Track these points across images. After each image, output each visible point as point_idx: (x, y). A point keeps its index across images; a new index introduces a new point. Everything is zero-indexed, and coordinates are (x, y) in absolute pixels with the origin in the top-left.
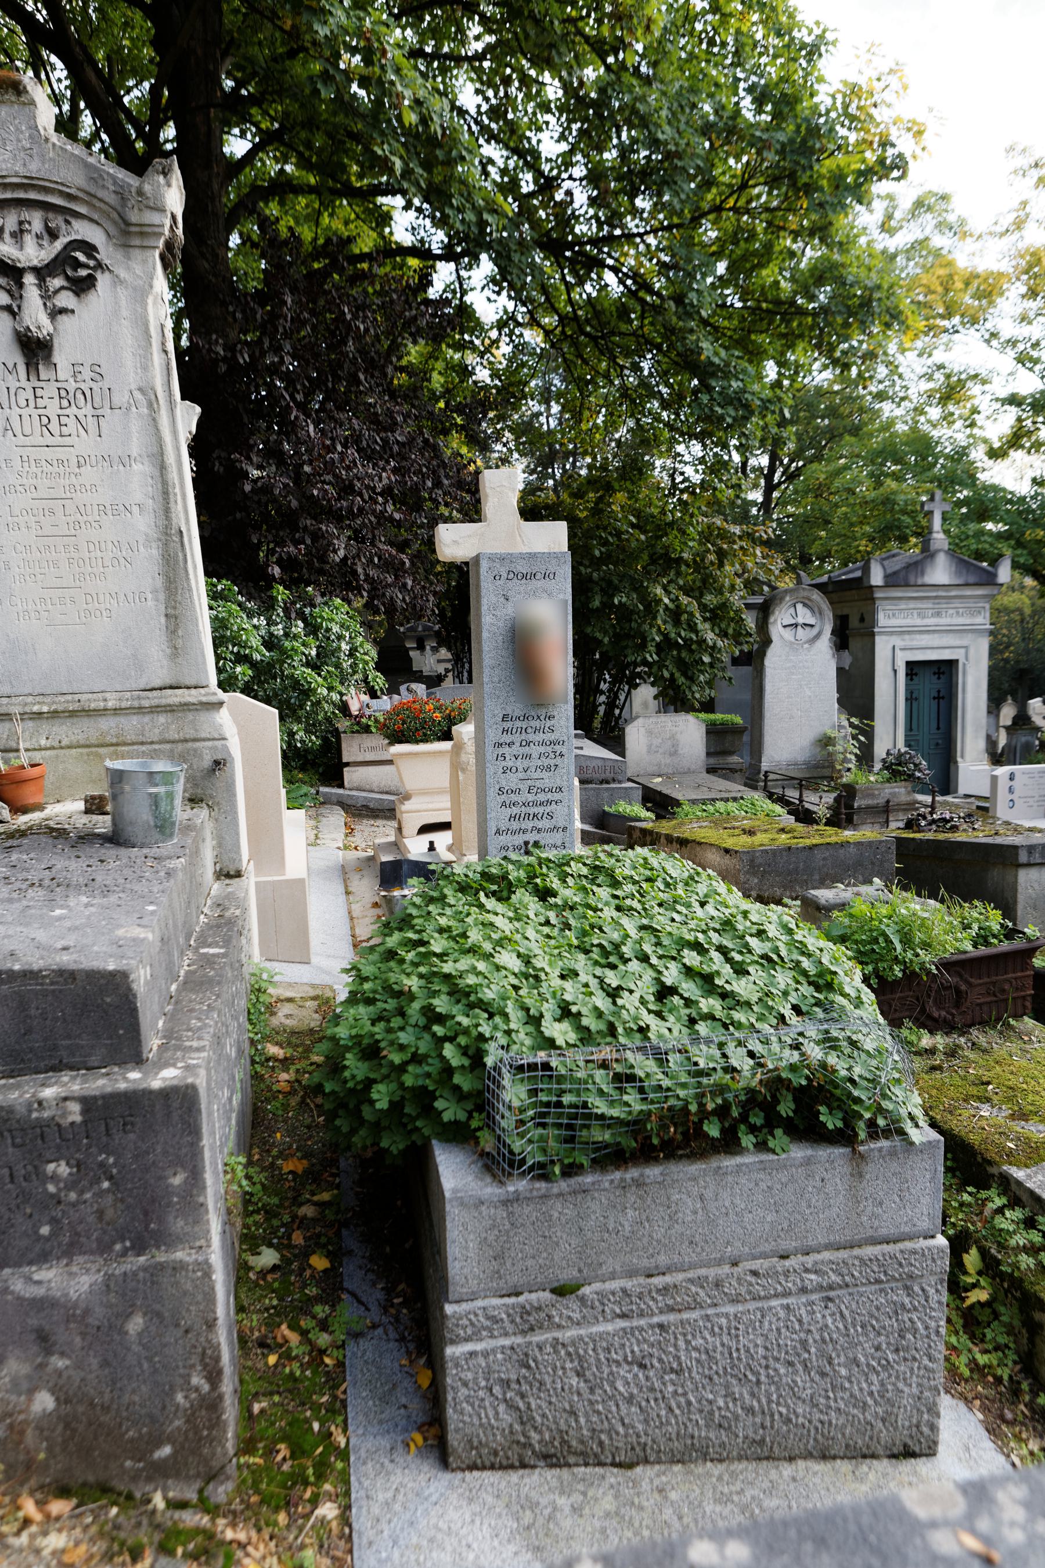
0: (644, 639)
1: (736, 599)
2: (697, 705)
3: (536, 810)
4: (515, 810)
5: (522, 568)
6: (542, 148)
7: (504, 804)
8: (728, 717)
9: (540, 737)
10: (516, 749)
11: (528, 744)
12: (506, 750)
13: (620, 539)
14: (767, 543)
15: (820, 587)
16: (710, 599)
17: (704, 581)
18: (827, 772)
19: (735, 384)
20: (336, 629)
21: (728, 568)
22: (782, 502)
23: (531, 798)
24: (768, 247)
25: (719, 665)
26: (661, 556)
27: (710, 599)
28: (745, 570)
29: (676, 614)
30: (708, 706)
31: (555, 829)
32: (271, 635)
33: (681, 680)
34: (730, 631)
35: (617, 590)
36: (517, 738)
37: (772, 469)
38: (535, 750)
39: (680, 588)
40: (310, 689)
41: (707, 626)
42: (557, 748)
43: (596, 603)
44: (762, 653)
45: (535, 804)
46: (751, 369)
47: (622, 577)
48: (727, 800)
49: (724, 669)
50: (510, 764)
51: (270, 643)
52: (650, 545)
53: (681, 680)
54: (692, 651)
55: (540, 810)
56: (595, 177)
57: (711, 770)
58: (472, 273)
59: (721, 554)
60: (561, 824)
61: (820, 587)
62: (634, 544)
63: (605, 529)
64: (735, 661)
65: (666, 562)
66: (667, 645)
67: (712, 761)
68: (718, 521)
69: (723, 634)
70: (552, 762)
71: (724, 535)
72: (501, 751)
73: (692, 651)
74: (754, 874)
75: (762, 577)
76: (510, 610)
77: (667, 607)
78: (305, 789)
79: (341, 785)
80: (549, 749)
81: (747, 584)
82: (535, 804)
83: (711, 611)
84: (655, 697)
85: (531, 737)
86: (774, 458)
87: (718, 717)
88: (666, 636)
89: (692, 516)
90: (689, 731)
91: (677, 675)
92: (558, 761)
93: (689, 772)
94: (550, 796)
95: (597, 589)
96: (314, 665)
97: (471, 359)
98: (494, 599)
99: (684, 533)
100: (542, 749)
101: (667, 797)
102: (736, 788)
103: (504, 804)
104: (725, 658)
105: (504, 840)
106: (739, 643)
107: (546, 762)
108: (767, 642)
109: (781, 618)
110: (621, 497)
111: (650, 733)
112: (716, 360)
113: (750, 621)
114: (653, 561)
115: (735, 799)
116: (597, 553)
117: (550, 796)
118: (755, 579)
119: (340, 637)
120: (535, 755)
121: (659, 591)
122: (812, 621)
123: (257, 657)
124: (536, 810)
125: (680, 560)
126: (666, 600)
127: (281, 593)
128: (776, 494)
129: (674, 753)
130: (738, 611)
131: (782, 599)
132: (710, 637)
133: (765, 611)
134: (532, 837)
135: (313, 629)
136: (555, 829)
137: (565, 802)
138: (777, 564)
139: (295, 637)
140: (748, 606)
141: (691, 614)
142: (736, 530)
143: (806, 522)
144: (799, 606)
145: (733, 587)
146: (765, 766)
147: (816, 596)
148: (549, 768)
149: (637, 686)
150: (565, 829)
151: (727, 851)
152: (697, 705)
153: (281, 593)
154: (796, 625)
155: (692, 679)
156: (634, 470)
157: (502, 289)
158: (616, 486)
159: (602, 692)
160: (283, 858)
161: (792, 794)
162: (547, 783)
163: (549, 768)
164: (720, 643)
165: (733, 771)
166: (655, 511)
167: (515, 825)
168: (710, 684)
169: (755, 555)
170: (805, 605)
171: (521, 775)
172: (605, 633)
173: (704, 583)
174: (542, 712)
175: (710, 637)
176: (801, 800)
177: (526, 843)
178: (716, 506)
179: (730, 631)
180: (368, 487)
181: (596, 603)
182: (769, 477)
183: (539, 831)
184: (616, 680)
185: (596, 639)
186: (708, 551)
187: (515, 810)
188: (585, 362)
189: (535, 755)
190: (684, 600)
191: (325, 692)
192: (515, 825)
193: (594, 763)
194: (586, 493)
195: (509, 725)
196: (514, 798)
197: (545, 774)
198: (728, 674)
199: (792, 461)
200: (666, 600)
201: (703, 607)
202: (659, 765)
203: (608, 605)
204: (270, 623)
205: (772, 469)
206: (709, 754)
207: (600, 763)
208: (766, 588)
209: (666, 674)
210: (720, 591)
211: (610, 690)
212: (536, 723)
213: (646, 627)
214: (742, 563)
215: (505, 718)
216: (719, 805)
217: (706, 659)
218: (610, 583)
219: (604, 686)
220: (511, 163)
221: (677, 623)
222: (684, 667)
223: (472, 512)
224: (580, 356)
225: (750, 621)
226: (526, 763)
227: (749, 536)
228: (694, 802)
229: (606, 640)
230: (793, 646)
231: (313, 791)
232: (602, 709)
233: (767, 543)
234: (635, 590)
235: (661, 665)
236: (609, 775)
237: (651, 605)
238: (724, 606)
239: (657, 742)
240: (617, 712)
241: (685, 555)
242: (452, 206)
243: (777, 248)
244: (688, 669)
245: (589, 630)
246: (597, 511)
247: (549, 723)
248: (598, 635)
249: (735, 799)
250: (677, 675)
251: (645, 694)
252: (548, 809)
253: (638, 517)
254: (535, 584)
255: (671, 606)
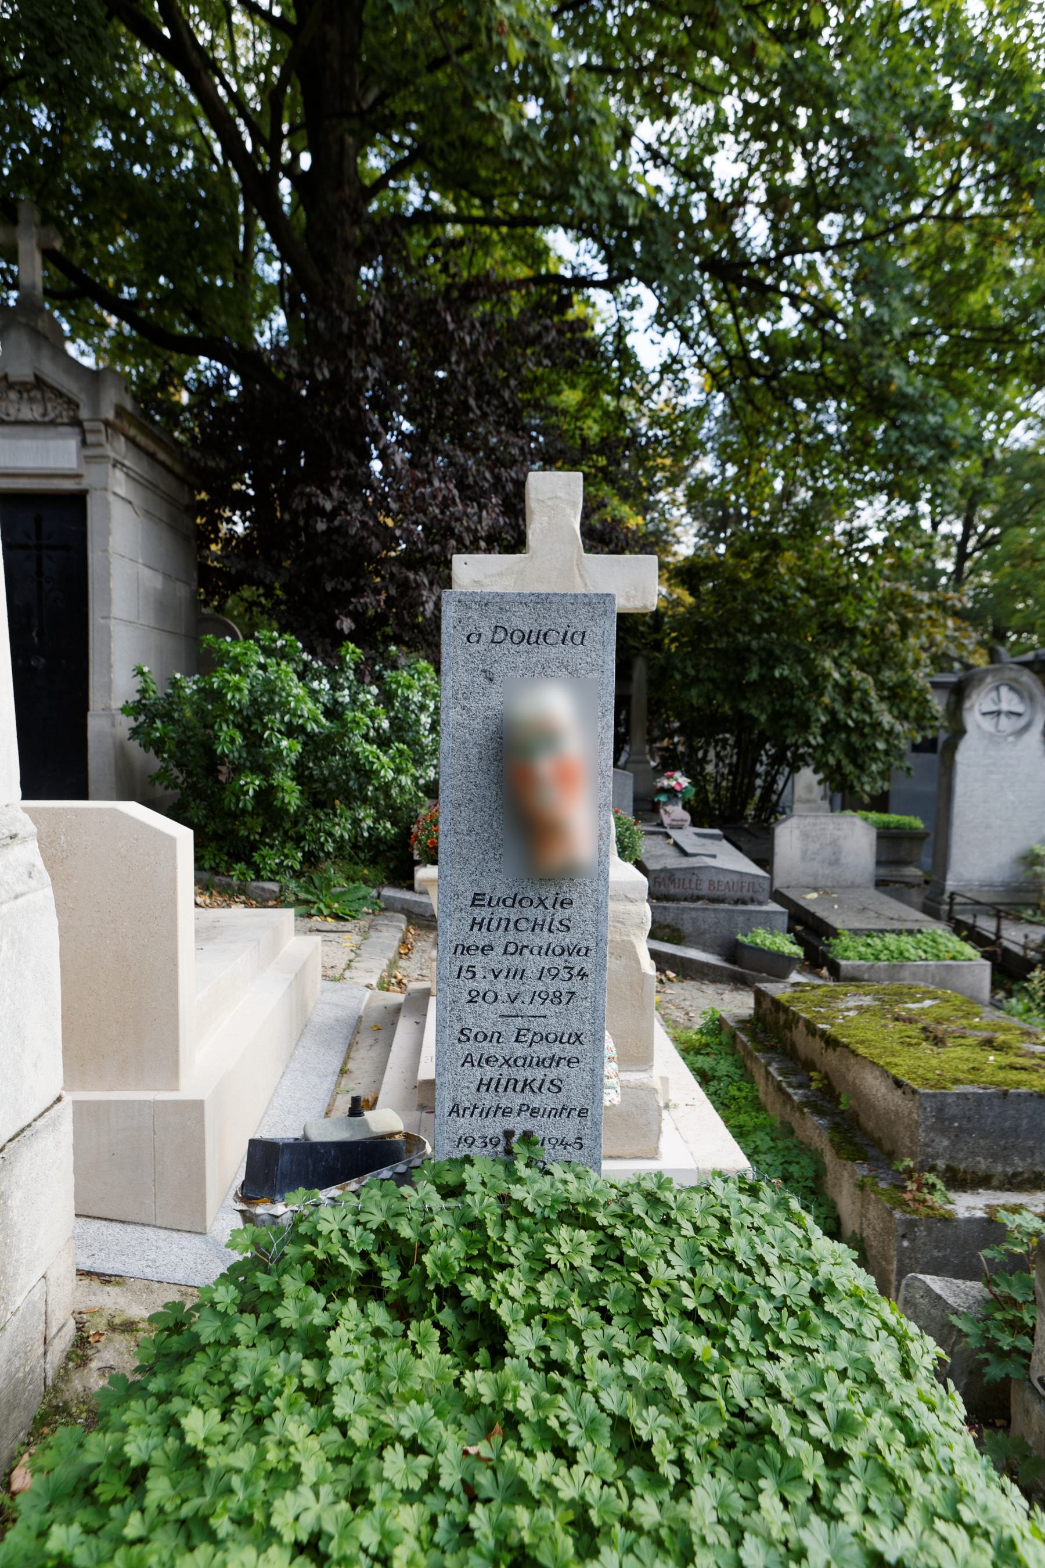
0: (808, 718)
1: (921, 677)
2: (866, 799)
3: (529, 1074)
4: (489, 1072)
5: (521, 621)
6: (715, 169)
7: (468, 1060)
8: (905, 819)
9: (542, 938)
10: (495, 960)
11: (520, 950)
12: (477, 960)
13: (785, 604)
14: (957, 614)
15: (1026, 665)
16: (889, 675)
17: (883, 655)
18: (1032, 898)
19: (932, 419)
20: (417, 697)
21: (912, 641)
22: (975, 571)
23: (520, 1050)
24: (979, 266)
25: (894, 752)
26: (833, 625)
27: (889, 675)
28: (932, 643)
29: (847, 692)
30: (880, 803)
31: (564, 1111)
32: (336, 702)
33: (849, 768)
34: (912, 714)
35: (779, 661)
36: (499, 939)
37: (966, 536)
38: (532, 963)
39: (854, 662)
40: (371, 771)
41: (884, 706)
42: (576, 961)
43: (754, 675)
44: (952, 746)
45: (528, 1062)
46: (953, 403)
47: (786, 647)
48: (899, 933)
49: (901, 756)
50: (483, 986)
51: (333, 712)
52: (820, 610)
53: (849, 768)
54: (863, 736)
55: (538, 1074)
56: (777, 200)
57: (881, 884)
58: (634, 313)
59: (905, 625)
60: (576, 1103)
61: (1026, 665)
62: (801, 611)
63: (769, 592)
64: (916, 748)
65: (839, 632)
66: (833, 727)
67: (884, 872)
68: (903, 587)
69: (903, 717)
70: (564, 987)
71: (909, 602)
72: (467, 961)
73: (863, 736)
74: (944, 1132)
75: (953, 652)
76: (494, 697)
77: (836, 682)
78: (364, 890)
79: (411, 888)
80: (559, 962)
81: (935, 660)
82: (528, 1062)
83: (890, 689)
84: (820, 782)
85: (525, 938)
86: (969, 526)
87: (892, 818)
88: (832, 713)
89: (871, 579)
90: (856, 837)
91: (845, 762)
92: (576, 985)
93: (852, 886)
94: (556, 1049)
95: (755, 659)
96: (383, 742)
97: (629, 405)
98: (465, 678)
99: (859, 599)
100: (546, 962)
101: (821, 922)
102: (914, 916)
103: (468, 1060)
104: (904, 745)
105: (464, 1124)
106: (921, 728)
107: (553, 986)
108: (959, 732)
109: (979, 705)
110: (790, 556)
111: (805, 836)
112: (910, 390)
113: (938, 703)
114: (823, 628)
115: (910, 932)
116: (758, 619)
117: (556, 1049)
118: (945, 655)
119: (423, 707)
120: (532, 972)
121: (828, 664)
122: (1019, 708)
123: (311, 726)
124: (529, 1074)
125: (854, 630)
126: (836, 675)
127: (352, 652)
128: (968, 564)
129: (835, 861)
130: (922, 691)
131: (981, 680)
132: (887, 719)
133: (959, 693)
134: (519, 1124)
135: (387, 698)
136: (564, 1111)
137: (586, 1062)
138: (971, 638)
139: (363, 706)
140: (935, 685)
141: (865, 693)
142: (925, 597)
143: (1003, 593)
144: (1004, 690)
145: (917, 664)
146: (951, 885)
147: (1027, 677)
148: (557, 998)
149: (798, 769)
150: (583, 1113)
151: (898, 1084)
152: (866, 799)
153: (352, 652)
154: (998, 713)
155: (862, 768)
156: (807, 523)
157: (667, 330)
158: (784, 544)
159: (759, 775)
160: (176, 1063)
161: (987, 925)
162: (553, 1025)
163: (557, 998)
164: (898, 728)
165: (909, 885)
166: (827, 573)
167: (488, 1100)
168: (884, 775)
169: (945, 626)
170: (1012, 688)
171: (503, 1008)
172: (763, 710)
173: (883, 656)
174: (549, 893)
175: (887, 719)
176: (998, 936)
177: (509, 1134)
178: (901, 568)
179: (912, 714)
180: (468, 529)
181: (754, 675)
182: (962, 545)
183: (534, 1112)
184: (777, 760)
185: (750, 716)
186: (889, 620)
187: (489, 1072)
188: (757, 409)
189: (532, 972)
190: (857, 675)
191: (390, 775)
192: (488, 1100)
193: (728, 878)
194: (751, 552)
195: (484, 913)
196: (489, 1048)
197: (549, 1009)
198: (907, 763)
199: (987, 529)
200: (836, 675)
201: (880, 685)
202: (815, 875)
203: (766, 678)
204: (335, 687)
205: (966, 536)
206: (879, 863)
207: (736, 878)
208: (957, 665)
209: (832, 761)
210: (901, 667)
211: (767, 773)
212: (535, 913)
213: (811, 705)
214: (929, 636)
215: (477, 900)
216: (890, 939)
217: (881, 745)
218: (770, 653)
219: (760, 769)
220: (682, 190)
221: (848, 701)
222: (854, 754)
223: (511, 539)
224: (750, 401)
225: (938, 703)
226: (514, 986)
227: (940, 605)
228: (856, 932)
229: (763, 718)
230: (994, 739)
231: (374, 893)
232: (758, 792)
233: (957, 614)
234: (800, 661)
235: (825, 749)
236: (746, 894)
237: (817, 681)
238: (906, 684)
239: (814, 847)
240: (774, 797)
241: (862, 624)
242: (577, 184)
243: (989, 267)
244: (857, 756)
245: (743, 706)
246: (760, 573)
247: (560, 914)
248: (755, 712)
249: (910, 932)
250: (845, 762)
251: (807, 780)
252: (553, 1073)
253: (808, 580)
254: (553, 652)
255: (842, 681)
